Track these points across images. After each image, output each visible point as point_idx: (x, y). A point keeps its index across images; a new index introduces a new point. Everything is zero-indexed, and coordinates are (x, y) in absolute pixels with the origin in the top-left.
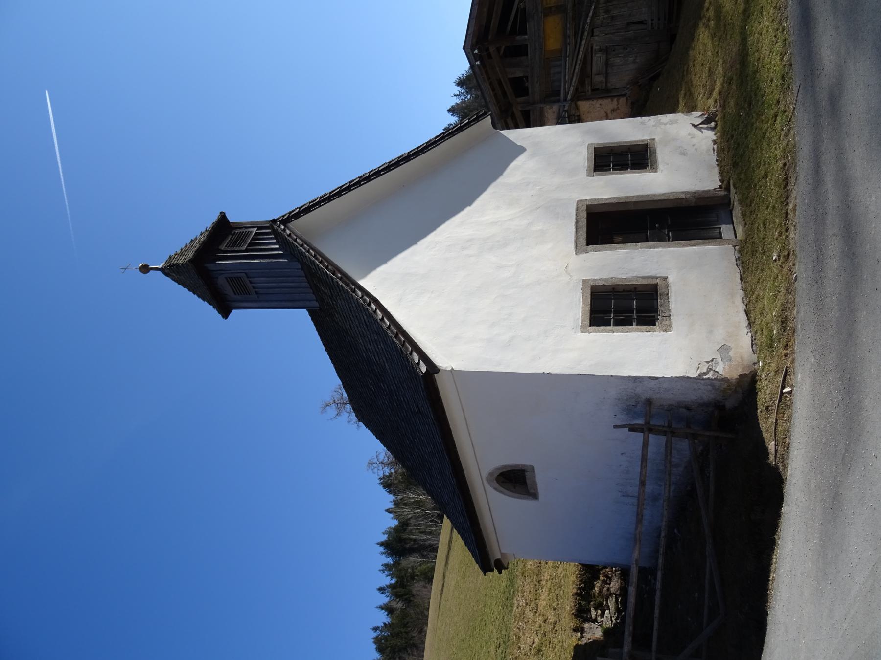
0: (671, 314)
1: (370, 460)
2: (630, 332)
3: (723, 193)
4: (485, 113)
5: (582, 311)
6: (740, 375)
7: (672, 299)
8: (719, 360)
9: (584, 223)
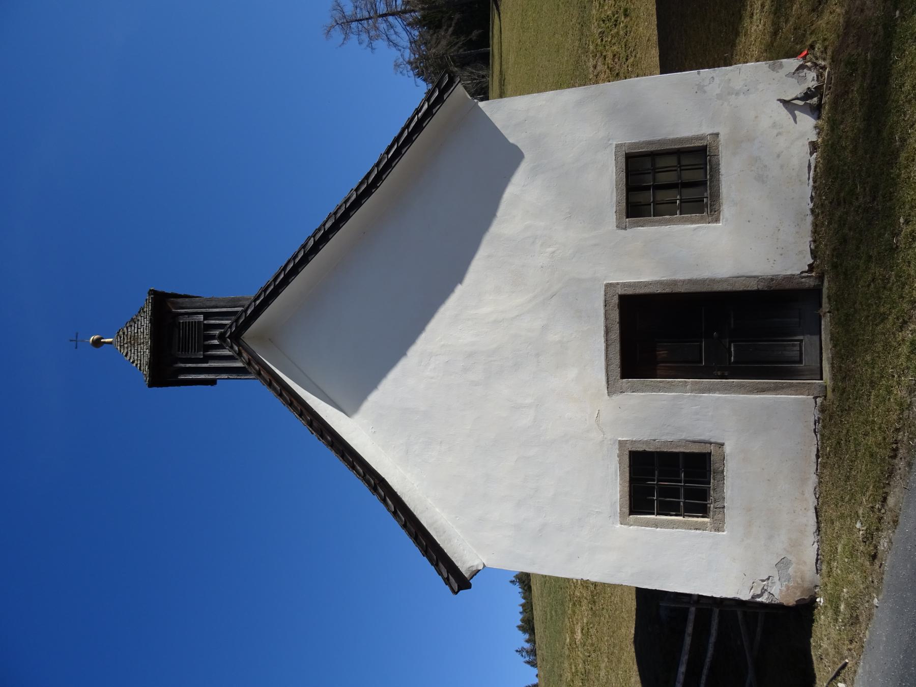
0: (726, 505)
1: (395, 61)
2: (676, 528)
3: (810, 283)
4: (451, 82)
5: (620, 491)
6: (798, 600)
7: (728, 482)
8: (776, 579)
9: (615, 335)
